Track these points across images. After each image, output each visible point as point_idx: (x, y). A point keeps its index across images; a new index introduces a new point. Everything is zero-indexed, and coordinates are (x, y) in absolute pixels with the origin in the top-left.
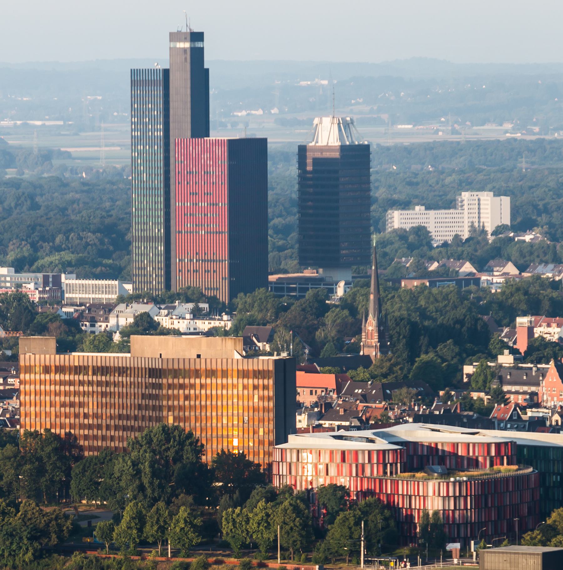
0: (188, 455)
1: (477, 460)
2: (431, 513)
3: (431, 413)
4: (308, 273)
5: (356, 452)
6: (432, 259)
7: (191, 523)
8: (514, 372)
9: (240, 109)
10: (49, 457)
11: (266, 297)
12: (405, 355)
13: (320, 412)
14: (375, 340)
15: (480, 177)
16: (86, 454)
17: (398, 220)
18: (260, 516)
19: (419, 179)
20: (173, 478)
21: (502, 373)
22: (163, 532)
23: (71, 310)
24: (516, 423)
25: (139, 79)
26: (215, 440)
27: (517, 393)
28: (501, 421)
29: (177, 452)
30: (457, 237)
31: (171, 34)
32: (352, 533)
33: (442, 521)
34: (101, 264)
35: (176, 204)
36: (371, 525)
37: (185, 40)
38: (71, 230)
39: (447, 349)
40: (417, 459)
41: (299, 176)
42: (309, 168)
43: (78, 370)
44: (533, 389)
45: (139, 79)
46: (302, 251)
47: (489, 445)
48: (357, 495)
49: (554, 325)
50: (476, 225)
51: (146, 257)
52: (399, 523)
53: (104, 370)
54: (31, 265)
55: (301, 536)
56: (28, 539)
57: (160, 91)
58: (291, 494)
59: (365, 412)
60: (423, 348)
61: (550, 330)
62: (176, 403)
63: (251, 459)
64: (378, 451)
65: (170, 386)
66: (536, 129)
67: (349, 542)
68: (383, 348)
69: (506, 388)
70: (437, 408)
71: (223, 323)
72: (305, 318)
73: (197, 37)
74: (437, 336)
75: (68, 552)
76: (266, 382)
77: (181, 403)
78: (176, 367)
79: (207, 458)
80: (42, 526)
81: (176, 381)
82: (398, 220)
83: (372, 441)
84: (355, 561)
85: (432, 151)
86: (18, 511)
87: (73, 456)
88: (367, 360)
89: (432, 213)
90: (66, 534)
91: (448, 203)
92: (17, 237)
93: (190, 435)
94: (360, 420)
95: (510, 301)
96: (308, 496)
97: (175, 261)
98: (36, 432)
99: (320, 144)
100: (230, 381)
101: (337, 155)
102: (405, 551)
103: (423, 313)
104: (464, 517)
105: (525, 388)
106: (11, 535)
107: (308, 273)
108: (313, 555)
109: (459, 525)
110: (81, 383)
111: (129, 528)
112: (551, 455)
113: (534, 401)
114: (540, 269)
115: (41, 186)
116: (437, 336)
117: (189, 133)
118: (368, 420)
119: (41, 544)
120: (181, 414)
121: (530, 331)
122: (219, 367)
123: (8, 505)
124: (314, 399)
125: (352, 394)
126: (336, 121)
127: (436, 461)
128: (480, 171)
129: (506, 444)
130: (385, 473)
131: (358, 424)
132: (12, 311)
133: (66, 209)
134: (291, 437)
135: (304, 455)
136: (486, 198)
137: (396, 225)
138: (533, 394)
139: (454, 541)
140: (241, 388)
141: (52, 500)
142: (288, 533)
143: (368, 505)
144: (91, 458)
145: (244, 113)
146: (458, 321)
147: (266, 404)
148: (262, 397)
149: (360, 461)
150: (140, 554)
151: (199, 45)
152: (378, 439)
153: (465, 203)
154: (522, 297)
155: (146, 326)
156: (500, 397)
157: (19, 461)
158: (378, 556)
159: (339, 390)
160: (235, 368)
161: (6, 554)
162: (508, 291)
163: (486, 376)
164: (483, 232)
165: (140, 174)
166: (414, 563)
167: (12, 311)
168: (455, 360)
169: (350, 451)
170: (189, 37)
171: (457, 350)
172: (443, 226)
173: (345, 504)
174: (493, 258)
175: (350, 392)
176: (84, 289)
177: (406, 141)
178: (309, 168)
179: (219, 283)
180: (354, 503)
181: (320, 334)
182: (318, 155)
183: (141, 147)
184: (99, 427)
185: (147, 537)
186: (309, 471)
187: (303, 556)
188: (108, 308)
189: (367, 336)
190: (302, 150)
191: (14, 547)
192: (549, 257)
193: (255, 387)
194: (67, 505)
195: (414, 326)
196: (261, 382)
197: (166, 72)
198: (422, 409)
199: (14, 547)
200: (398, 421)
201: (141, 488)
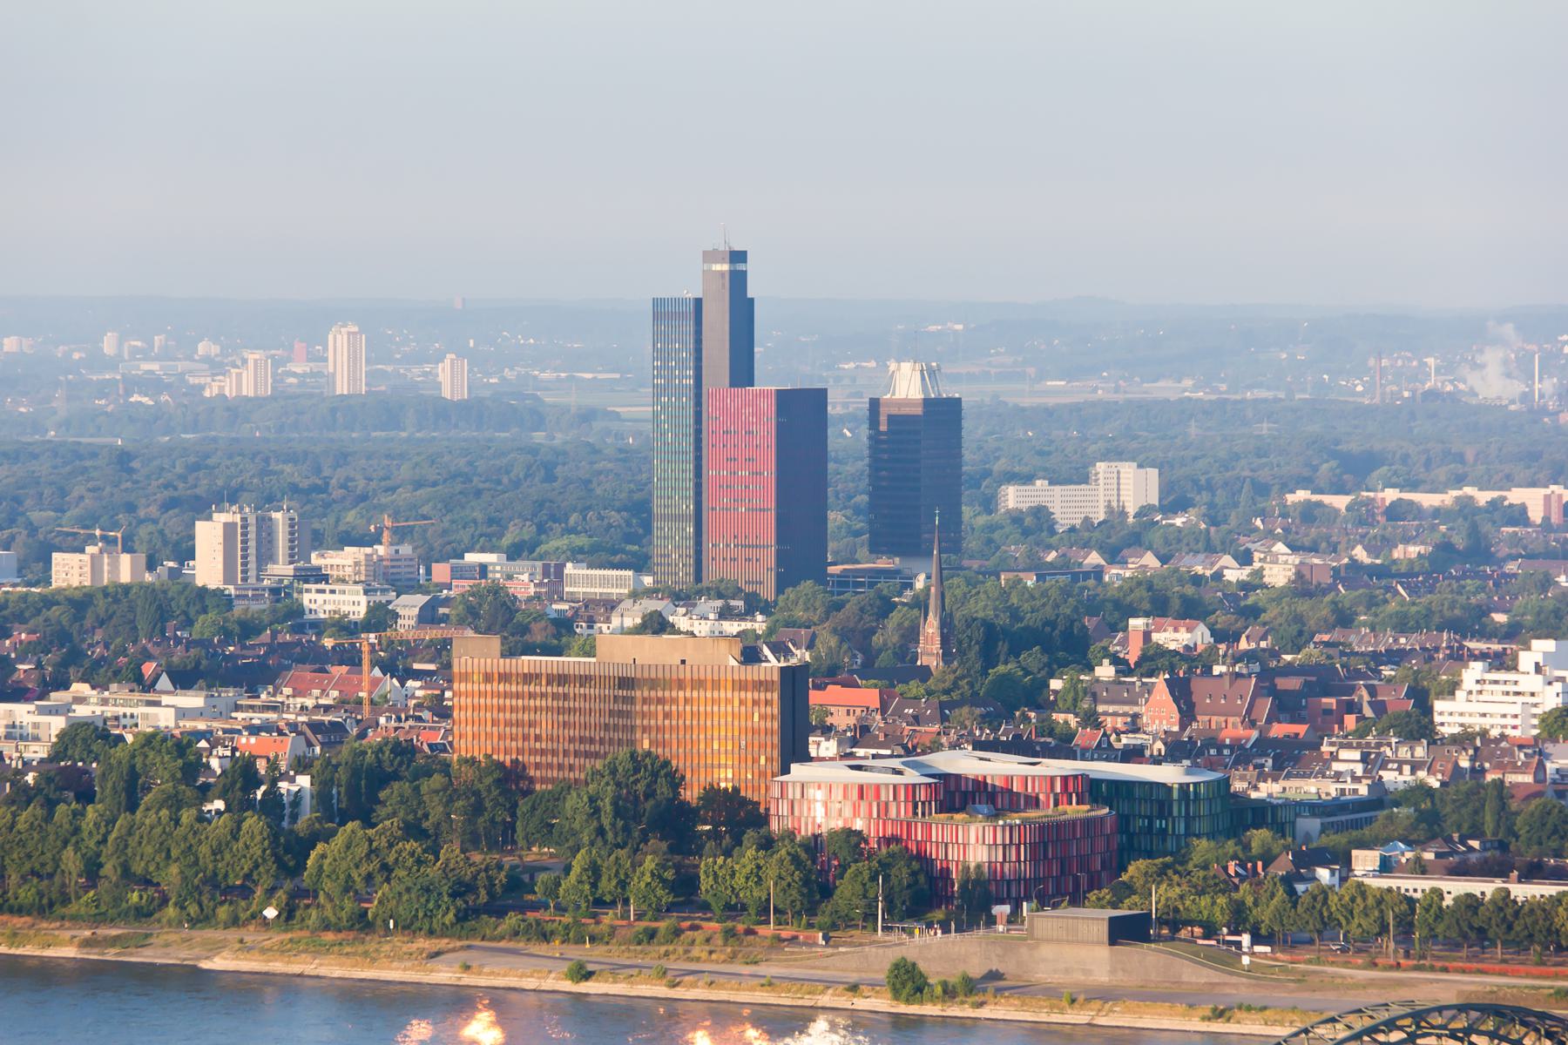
0: (663, 789)
1: (1037, 798)
2: (972, 866)
3: (996, 739)
4: (883, 563)
5: (877, 787)
6: (1050, 547)
7: (660, 877)
8: (1111, 687)
9: (848, 360)
10: (489, 791)
11: (814, 593)
12: (978, 666)
13: (854, 737)
14: (936, 647)
15: (1134, 445)
16: (538, 787)
17: (1013, 498)
18: (748, 870)
19: (1052, 448)
20: (644, 819)
21: (1097, 688)
22: (624, 888)
23: (565, 607)
24: (1106, 752)
26: (702, 770)
27: (1115, 714)
28: (1085, 750)
29: (648, 786)
30: (1087, 519)
32: (866, 891)
34: (623, 551)
35: (710, 473)
36: (894, 881)
37: (722, 261)
38: (589, 508)
39: (1033, 658)
40: (956, 796)
41: (870, 438)
42: (883, 428)
43: (528, 678)
44: (1136, 709)
45: (662, 311)
46: (874, 535)
47: (1052, 779)
48: (879, 843)
49: (1183, 630)
50: (1114, 504)
51: (671, 542)
52: (931, 879)
53: (562, 679)
54: (532, 551)
55: (802, 895)
56: (450, 895)
57: (690, 327)
58: (793, 840)
59: (910, 737)
60: (1002, 658)
61: (1177, 636)
62: (653, 722)
63: (749, 795)
64: (907, 786)
65: (645, 701)
66: (1223, 387)
67: (863, 902)
68: (947, 656)
69: (1101, 708)
70: (1006, 733)
71: (756, 626)
72: (861, 619)
73: (738, 257)
74: (1020, 642)
75: (501, 913)
76: (769, 695)
77: (660, 723)
78: (653, 675)
79: (691, 794)
80: (467, 878)
81: (653, 694)
82: (1013, 498)
83: (900, 773)
84: (870, 926)
85: (1077, 413)
86: (437, 859)
87: (521, 790)
88: (925, 673)
89: (1057, 488)
90: (498, 889)
91: (1081, 477)
92: (520, 516)
93: (667, 763)
94: (905, 747)
95: (1129, 599)
96: (814, 845)
97: (708, 545)
98: (473, 758)
100: (723, 695)
101: (919, 411)
102: (939, 914)
103: (1015, 615)
104: (1017, 872)
105: (1126, 708)
106: (428, 890)
107: (883, 563)
108: (815, 920)
109: (1009, 882)
110: (532, 696)
111: (580, 882)
112: (1137, 792)
113: (1134, 726)
114: (1188, 559)
115: (565, 453)
116: (1020, 642)
117: (727, 380)
118: (915, 748)
119: (466, 902)
120: (660, 736)
121: (1147, 635)
122: (709, 677)
123: (425, 851)
124: (852, 721)
125: (902, 716)
126: (918, 366)
127: (984, 798)
128: (1135, 438)
129: (1076, 777)
130: (915, 814)
131: (902, 752)
132: (486, 607)
133: (590, 481)
134: (794, 767)
135: (811, 791)
136: (1128, 470)
137: (1011, 504)
138: (1136, 716)
139: (1003, 903)
140: (736, 703)
141: (493, 845)
142: (784, 891)
143: (891, 855)
144: (543, 793)
145: (852, 365)
146: (1047, 623)
147: (769, 724)
148: (766, 715)
149: (883, 798)
150: (594, 916)
151: (741, 267)
152: (908, 770)
153: (1101, 476)
154: (1145, 594)
155: (656, 625)
156: (1091, 719)
157: (450, 794)
158: (901, 920)
159: (883, 709)
160: (729, 678)
161: (421, 915)
162: (1126, 587)
163: (1076, 693)
164: (1123, 513)
165: (663, 434)
166: (946, 931)
167: (486, 607)
168: (1043, 673)
169: (869, 785)
171: (1045, 659)
172: (1069, 506)
173: (862, 854)
174: (1129, 546)
175: (898, 713)
176: (589, 581)
177: (1051, 401)
178: (883, 428)
179: (762, 574)
180: (872, 854)
181: (877, 640)
182: (894, 411)
183: (664, 399)
184: (554, 753)
185: (603, 894)
186: (819, 812)
187: (804, 921)
188: (610, 605)
189: (926, 642)
190: (875, 404)
191: (431, 905)
192: (1201, 545)
193: (755, 703)
194: (511, 853)
195: (989, 626)
196: (762, 696)
198: (986, 734)
199: (431, 905)
200: (936, 747)
201: (601, 831)
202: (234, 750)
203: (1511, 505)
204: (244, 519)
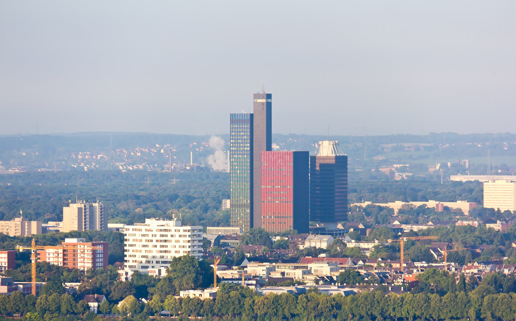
25: (234, 119)
31: (254, 95)
37: (263, 98)
42: (318, 168)
45: (234, 119)
73: (269, 96)
99: (322, 155)
101: (333, 161)
126: (331, 143)
151: (269, 101)
170: (265, 97)
178: (318, 168)
182: (322, 162)
197: (252, 115)
202: (404, 280)
203: (428, 208)
204: (85, 206)
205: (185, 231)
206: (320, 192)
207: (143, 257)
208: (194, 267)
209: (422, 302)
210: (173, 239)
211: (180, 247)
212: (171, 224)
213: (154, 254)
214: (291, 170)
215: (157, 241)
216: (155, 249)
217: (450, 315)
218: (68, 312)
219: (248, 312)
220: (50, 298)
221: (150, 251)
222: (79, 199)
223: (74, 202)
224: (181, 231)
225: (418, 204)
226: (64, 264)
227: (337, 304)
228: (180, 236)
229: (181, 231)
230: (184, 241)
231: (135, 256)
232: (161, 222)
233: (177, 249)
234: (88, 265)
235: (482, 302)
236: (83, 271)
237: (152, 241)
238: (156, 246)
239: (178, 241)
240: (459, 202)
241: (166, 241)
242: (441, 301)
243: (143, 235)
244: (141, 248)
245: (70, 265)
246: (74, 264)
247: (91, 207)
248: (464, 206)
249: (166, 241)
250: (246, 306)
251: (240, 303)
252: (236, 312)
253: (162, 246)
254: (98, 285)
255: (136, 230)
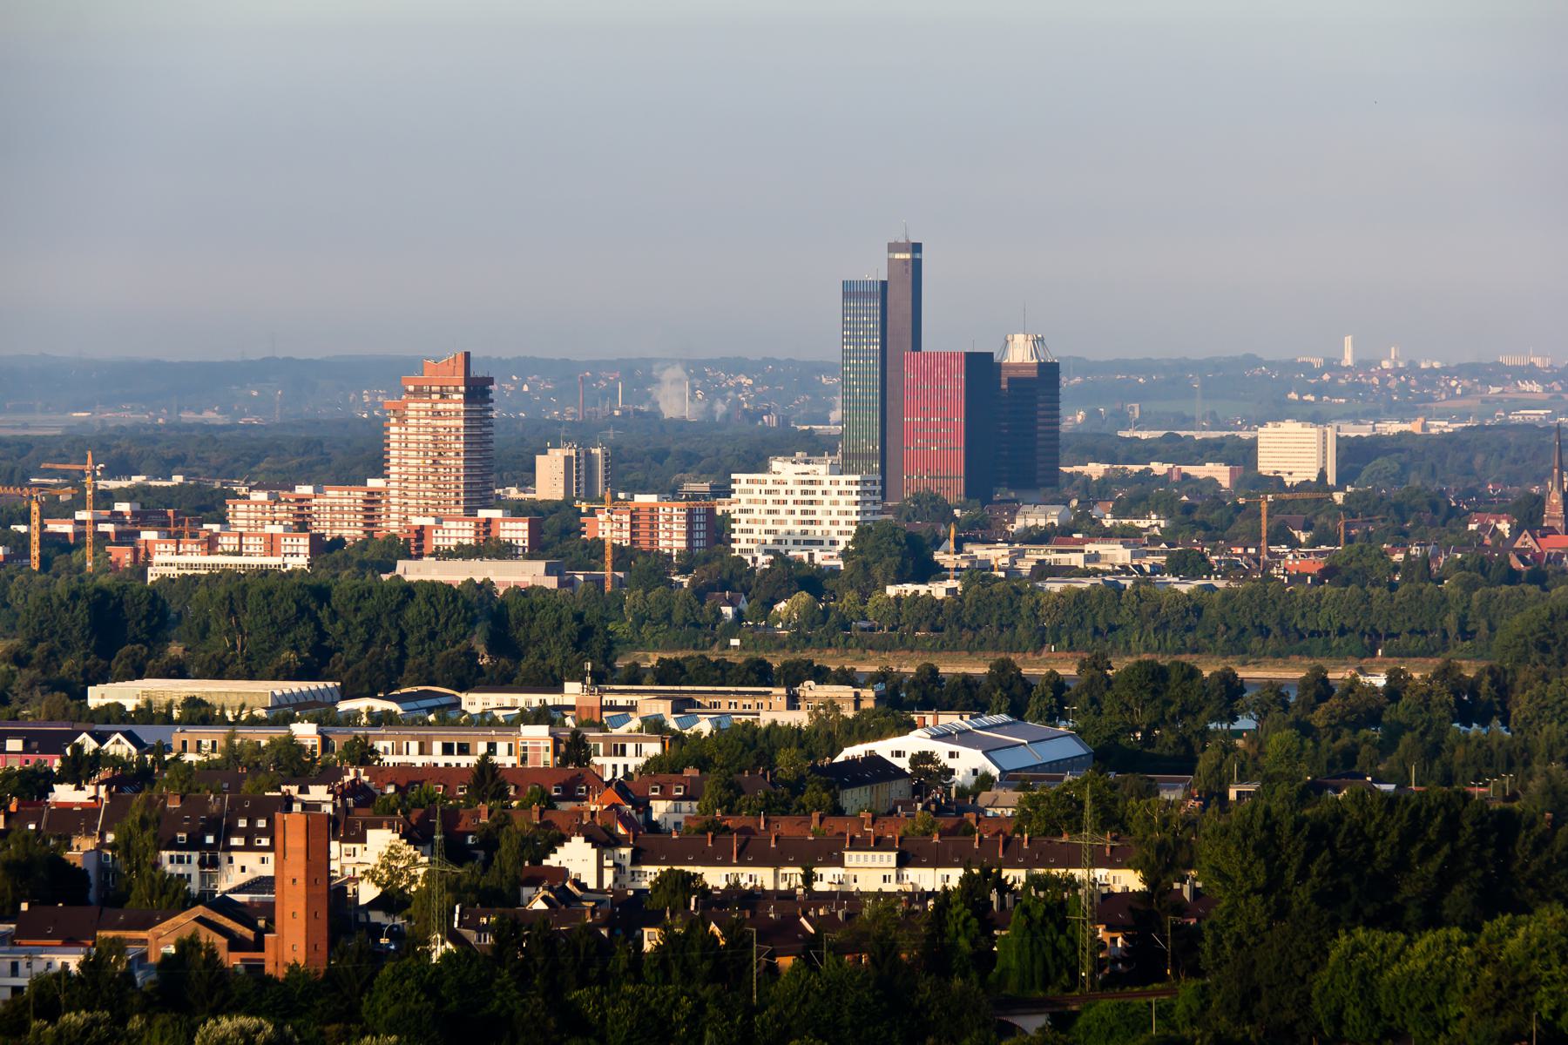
25: (851, 292)
33: (1084, 773)
37: (906, 251)
42: (1004, 386)
45: (851, 292)
73: (917, 248)
101: (1034, 373)
178: (1004, 386)
182: (1013, 373)
197: (884, 284)
205: (849, 483)
206: (1012, 425)
207: (768, 532)
208: (898, 543)
209: (1357, 602)
210: (826, 499)
211: (839, 513)
212: (821, 470)
213: (790, 526)
214: (961, 387)
215: (795, 502)
216: (790, 518)
217: (1409, 626)
218: (686, 620)
219: (1027, 621)
220: (652, 596)
221: (782, 522)
222: (567, 440)
223: (556, 446)
224: (842, 483)
225: (1136, 468)
226: (633, 542)
227: (1195, 606)
228: (840, 493)
229: (842, 483)
230: (847, 503)
231: (751, 531)
232: (802, 468)
233: (834, 517)
234: (680, 544)
235: (1469, 602)
236: (670, 556)
237: (785, 502)
238: (793, 512)
239: (836, 503)
240: (1209, 465)
241: (811, 502)
242: (1392, 600)
243: (769, 492)
244: (764, 516)
245: (644, 544)
246: (652, 543)
247: (588, 454)
248: (1220, 473)
249: (811, 502)
250: (1024, 611)
251: (1011, 604)
252: (1004, 621)
253: (804, 512)
254: (725, 575)
255: (753, 481)
